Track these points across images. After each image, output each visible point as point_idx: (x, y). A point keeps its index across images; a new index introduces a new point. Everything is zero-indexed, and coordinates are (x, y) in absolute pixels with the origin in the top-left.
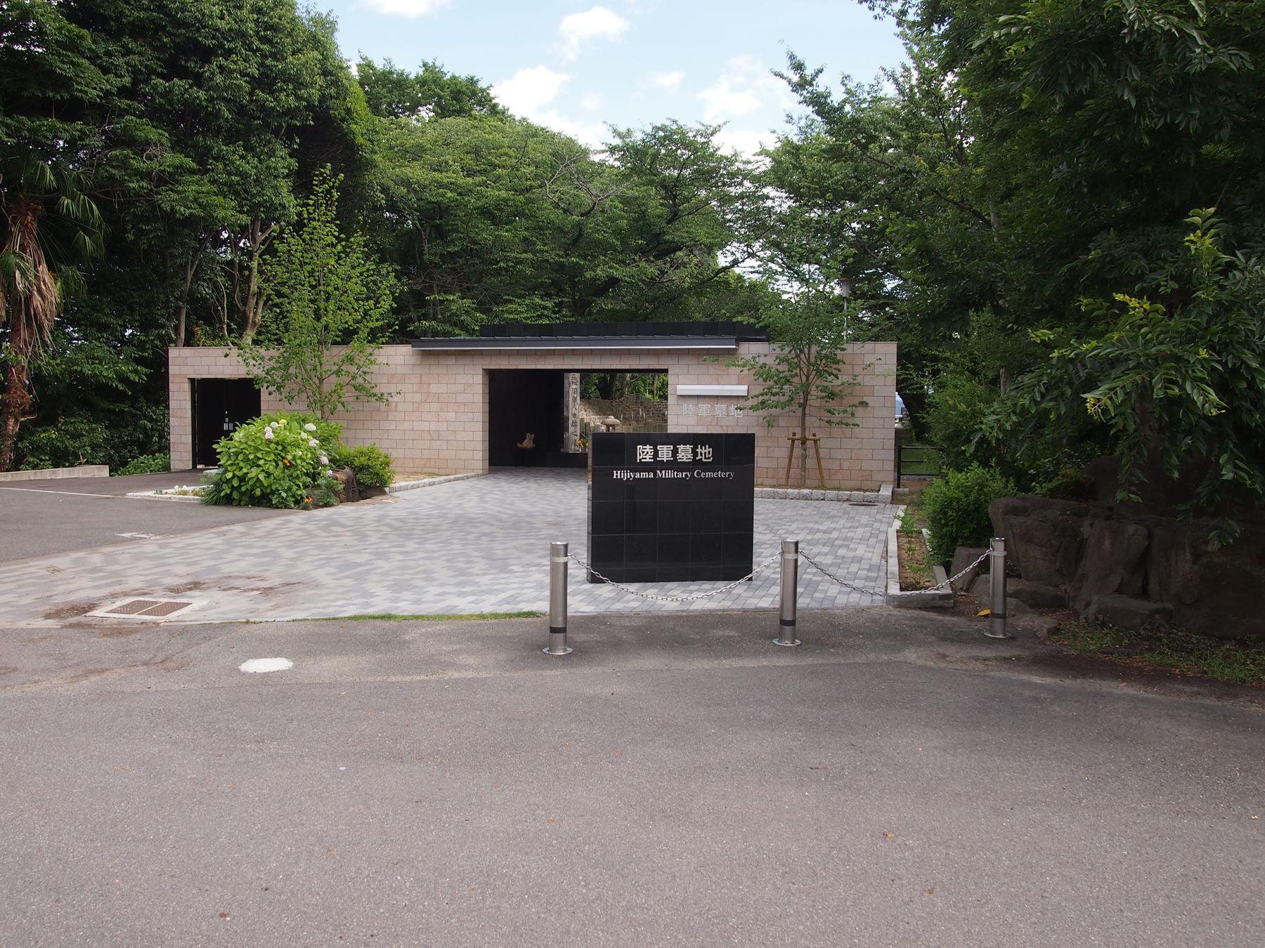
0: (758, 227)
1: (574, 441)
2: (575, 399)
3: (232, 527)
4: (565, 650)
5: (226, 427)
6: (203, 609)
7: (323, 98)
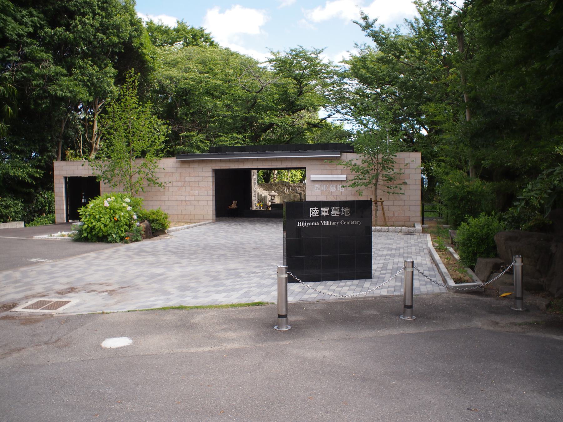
0: (340, 98)
1: (255, 206)
2: (255, 183)
3: (89, 254)
4: (287, 328)
5: (83, 201)
6: (77, 305)
7: (131, 37)
